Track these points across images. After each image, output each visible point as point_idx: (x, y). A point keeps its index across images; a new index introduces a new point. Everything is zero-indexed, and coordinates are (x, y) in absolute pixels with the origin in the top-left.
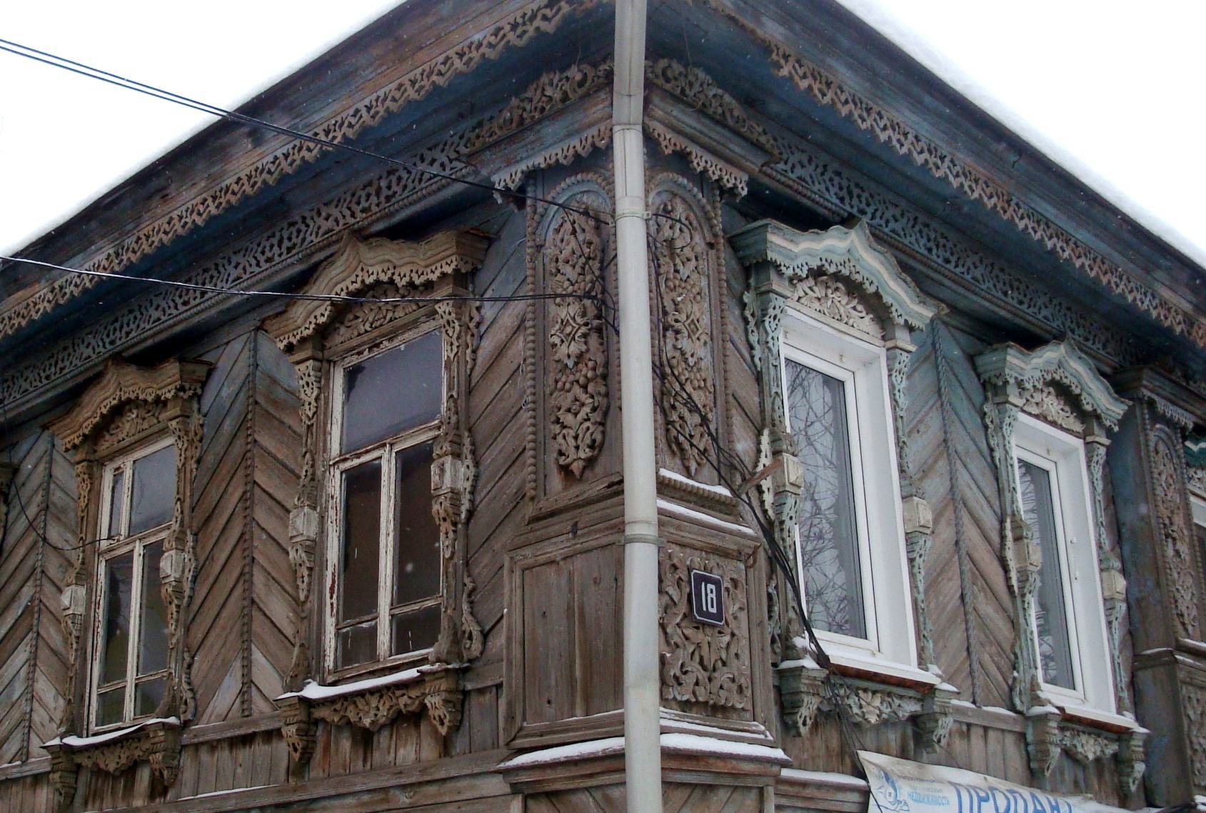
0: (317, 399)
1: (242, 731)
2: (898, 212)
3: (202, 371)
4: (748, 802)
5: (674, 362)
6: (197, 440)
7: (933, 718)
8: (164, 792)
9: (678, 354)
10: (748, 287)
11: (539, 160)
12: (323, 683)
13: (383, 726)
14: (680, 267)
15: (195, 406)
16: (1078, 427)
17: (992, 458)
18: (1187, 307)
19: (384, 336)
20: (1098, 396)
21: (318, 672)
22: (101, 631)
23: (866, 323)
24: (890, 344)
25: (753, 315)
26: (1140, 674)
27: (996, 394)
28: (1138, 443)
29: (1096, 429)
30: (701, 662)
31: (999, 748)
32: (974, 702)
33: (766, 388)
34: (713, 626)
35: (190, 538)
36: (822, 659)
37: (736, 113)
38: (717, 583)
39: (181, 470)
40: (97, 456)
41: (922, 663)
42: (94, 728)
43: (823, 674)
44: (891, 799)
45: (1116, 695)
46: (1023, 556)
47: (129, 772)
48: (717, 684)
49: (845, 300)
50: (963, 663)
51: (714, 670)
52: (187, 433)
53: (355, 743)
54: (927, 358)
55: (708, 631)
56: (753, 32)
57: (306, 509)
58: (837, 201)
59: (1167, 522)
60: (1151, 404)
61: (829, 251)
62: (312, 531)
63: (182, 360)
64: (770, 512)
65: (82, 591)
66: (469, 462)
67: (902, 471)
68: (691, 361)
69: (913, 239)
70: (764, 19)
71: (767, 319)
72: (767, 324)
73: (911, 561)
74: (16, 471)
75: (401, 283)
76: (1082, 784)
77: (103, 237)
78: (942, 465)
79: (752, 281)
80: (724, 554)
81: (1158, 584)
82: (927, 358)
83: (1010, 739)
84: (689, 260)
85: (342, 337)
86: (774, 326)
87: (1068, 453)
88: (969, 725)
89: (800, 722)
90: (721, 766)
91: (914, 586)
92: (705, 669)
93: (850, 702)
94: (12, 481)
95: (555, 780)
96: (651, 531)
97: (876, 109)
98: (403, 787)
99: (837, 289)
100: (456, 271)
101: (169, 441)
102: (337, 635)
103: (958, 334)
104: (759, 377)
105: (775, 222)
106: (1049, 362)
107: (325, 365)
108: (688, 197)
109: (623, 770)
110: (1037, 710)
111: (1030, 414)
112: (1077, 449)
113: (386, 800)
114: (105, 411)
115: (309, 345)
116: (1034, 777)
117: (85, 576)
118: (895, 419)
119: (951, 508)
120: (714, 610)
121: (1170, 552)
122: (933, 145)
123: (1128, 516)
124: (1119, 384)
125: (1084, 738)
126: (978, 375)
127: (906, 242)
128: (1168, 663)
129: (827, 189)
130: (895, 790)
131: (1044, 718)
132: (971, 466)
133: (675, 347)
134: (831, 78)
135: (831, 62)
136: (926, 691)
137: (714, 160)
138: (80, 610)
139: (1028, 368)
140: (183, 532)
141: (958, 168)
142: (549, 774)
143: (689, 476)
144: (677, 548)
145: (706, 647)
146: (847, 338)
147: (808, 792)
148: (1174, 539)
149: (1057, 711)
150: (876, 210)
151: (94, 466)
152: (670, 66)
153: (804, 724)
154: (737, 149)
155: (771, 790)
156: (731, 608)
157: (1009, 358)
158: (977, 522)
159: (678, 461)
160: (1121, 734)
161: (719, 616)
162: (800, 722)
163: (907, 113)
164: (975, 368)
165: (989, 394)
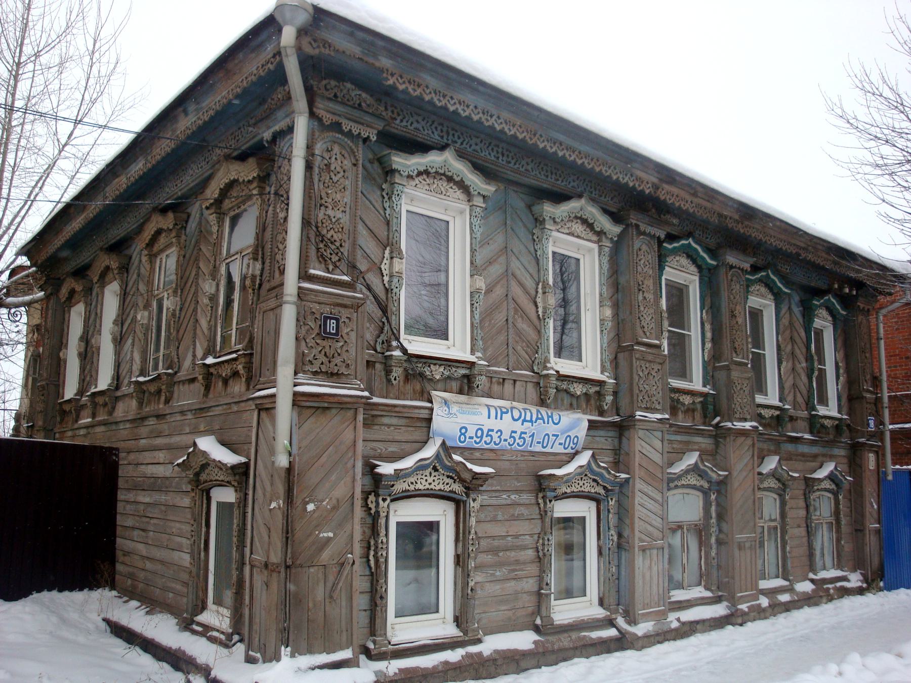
0: (218, 231)
1: (191, 377)
2: (478, 141)
3: (185, 216)
4: (349, 414)
5: (324, 221)
6: (183, 247)
7: (474, 376)
8: (168, 403)
9: (326, 217)
10: (386, 181)
11: (277, 128)
12: (215, 358)
13: (230, 377)
14: (333, 177)
15: (183, 232)
16: (595, 238)
17: (536, 255)
18: (655, 180)
19: (241, 203)
20: (604, 222)
21: (213, 352)
22: (154, 331)
23: (459, 194)
24: (471, 204)
25: (387, 194)
26: (619, 354)
27: (540, 225)
28: (629, 245)
29: (604, 239)
30: (325, 355)
31: (523, 389)
32: (508, 369)
33: (391, 228)
34: (333, 338)
35: (179, 291)
36: (404, 351)
37: (368, 102)
38: (337, 320)
39: (178, 261)
40: (154, 252)
41: (473, 352)
42: (151, 373)
43: (405, 357)
44: (447, 412)
45: (601, 365)
46: (545, 301)
47: (159, 392)
48: (333, 364)
49: (445, 184)
50: (504, 351)
51: (333, 357)
52: (179, 244)
53: (223, 383)
54: (500, 208)
55: (329, 340)
56: (373, 64)
57: (210, 281)
58: (439, 138)
59: (641, 283)
60: (637, 226)
61: (432, 162)
62: (213, 290)
63: (174, 212)
64: (387, 285)
65: (146, 314)
66: (260, 262)
67: (472, 263)
68: (334, 220)
69: (487, 153)
70: (380, 57)
71: (394, 196)
72: (393, 198)
73: (472, 305)
74: (130, 258)
75: (241, 180)
76: (575, 406)
77: (141, 155)
78: (502, 259)
79: (388, 179)
80: (345, 306)
81: (631, 313)
82: (500, 208)
83: (530, 387)
84: (338, 173)
85: (227, 204)
86: (397, 199)
87: (590, 250)
88: (504, 379)
89: (393, 379)
90: (332, 400)
91: (472, 316)
92: (327, 357)
93: (425, 369)
94: (129, 262)
95: (266, 403)
96: (294, 299)
97: (449, 95)
98: (235, 403)
99: (441, 179)
100: (258, 175)
101: (174, 249)
102: (221, 336)
103: (522, 195)
104: (388, 223)
105: (394, 151)
106: (575, 208)
107: (222, 216)
108: (343, 143)
109: (275, 402)
110: (545, 372)
111: (563, 233)
112: (593, 249)
113: (230, 408)
114: (153, 233)
115: (214, 207)
116: (542, 403)
117: (147, 306)
118: (471, 239)
119: (505, 279)
120: (334, 332)
121: (641, 298)
122: (486, 110)
123: (622, 280)
124: (616, 218)
125: (575, 385)
126: (533, 215)
127: (482, 155)
128: (630, 350)
129: (433, 133)
130: (449, 408)
131: (547, 376)
132: (522, 259)
133: (325, 214)
134: (421, 82)
135: (422, 75)
136: (472, 365)
137: (353, 124)
138: (145, 322)
139: (558, 211)
140: (176, 289)
141: (502, 120)
142: (265, 401)
143: (329, 272)
144: (317, 305)
145: (327, 348)
146: (446, 202)
147: (397, 409)
148: (643, 292)
149: (555, 373)
150: (464, 141)
151: (152, 257)
152: (329, 83)
153: (395, 379)
154: (369, 119)
155: (361, 410)
156: (344, 330)
157: (545, 208)
158: (521, 285)
159: (323, 266)
160: (601, 383)
161: (337, 334)
162: (393, 379)
163: (469, 96)
164: (531, 211)
165: (538, 225)
